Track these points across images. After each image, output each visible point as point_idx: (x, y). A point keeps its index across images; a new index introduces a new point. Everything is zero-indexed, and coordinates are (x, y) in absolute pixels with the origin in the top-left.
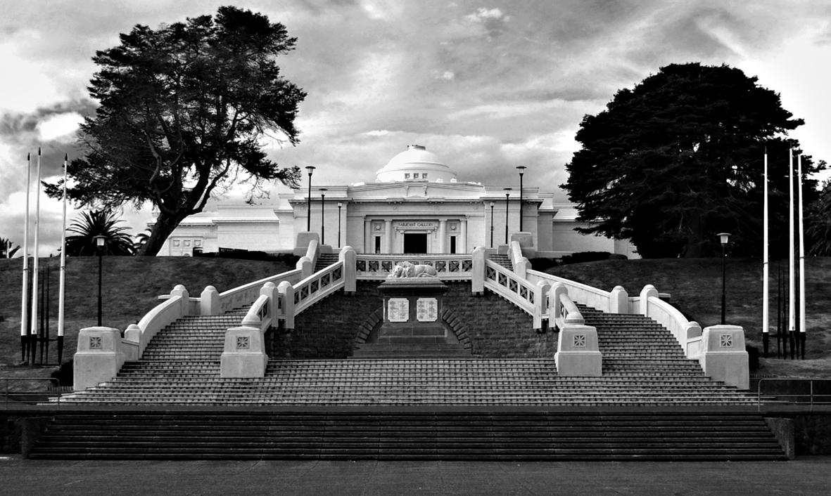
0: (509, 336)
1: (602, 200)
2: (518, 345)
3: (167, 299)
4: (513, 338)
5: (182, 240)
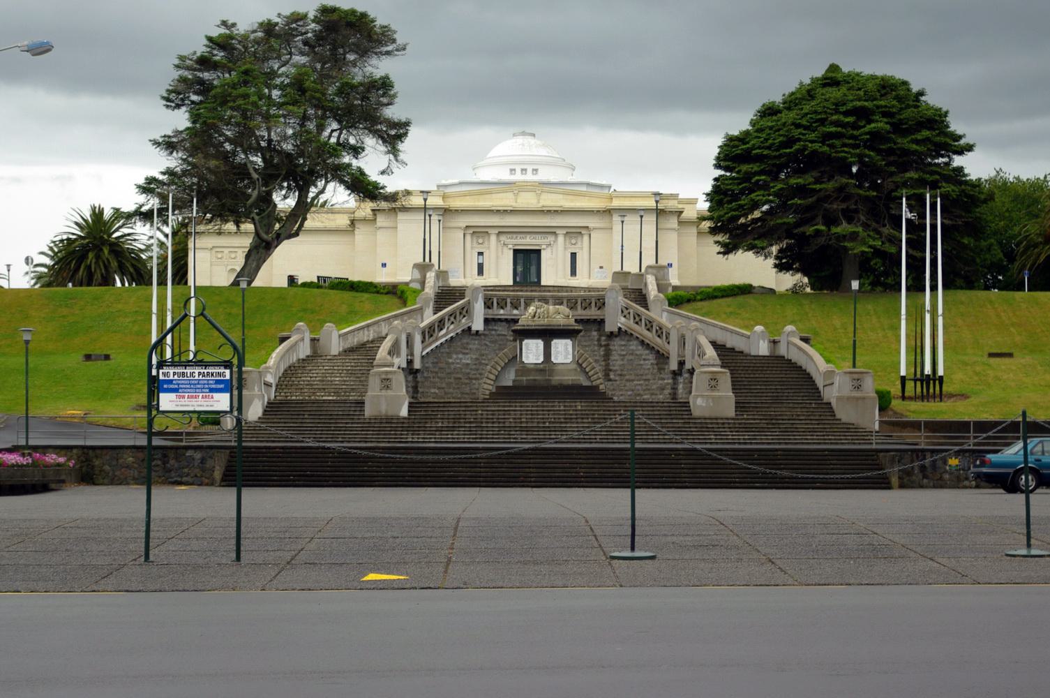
0: (644, 377)
1: (750, 229)
2: (654, 387)
4: (648, 380)
5: (226, 251)
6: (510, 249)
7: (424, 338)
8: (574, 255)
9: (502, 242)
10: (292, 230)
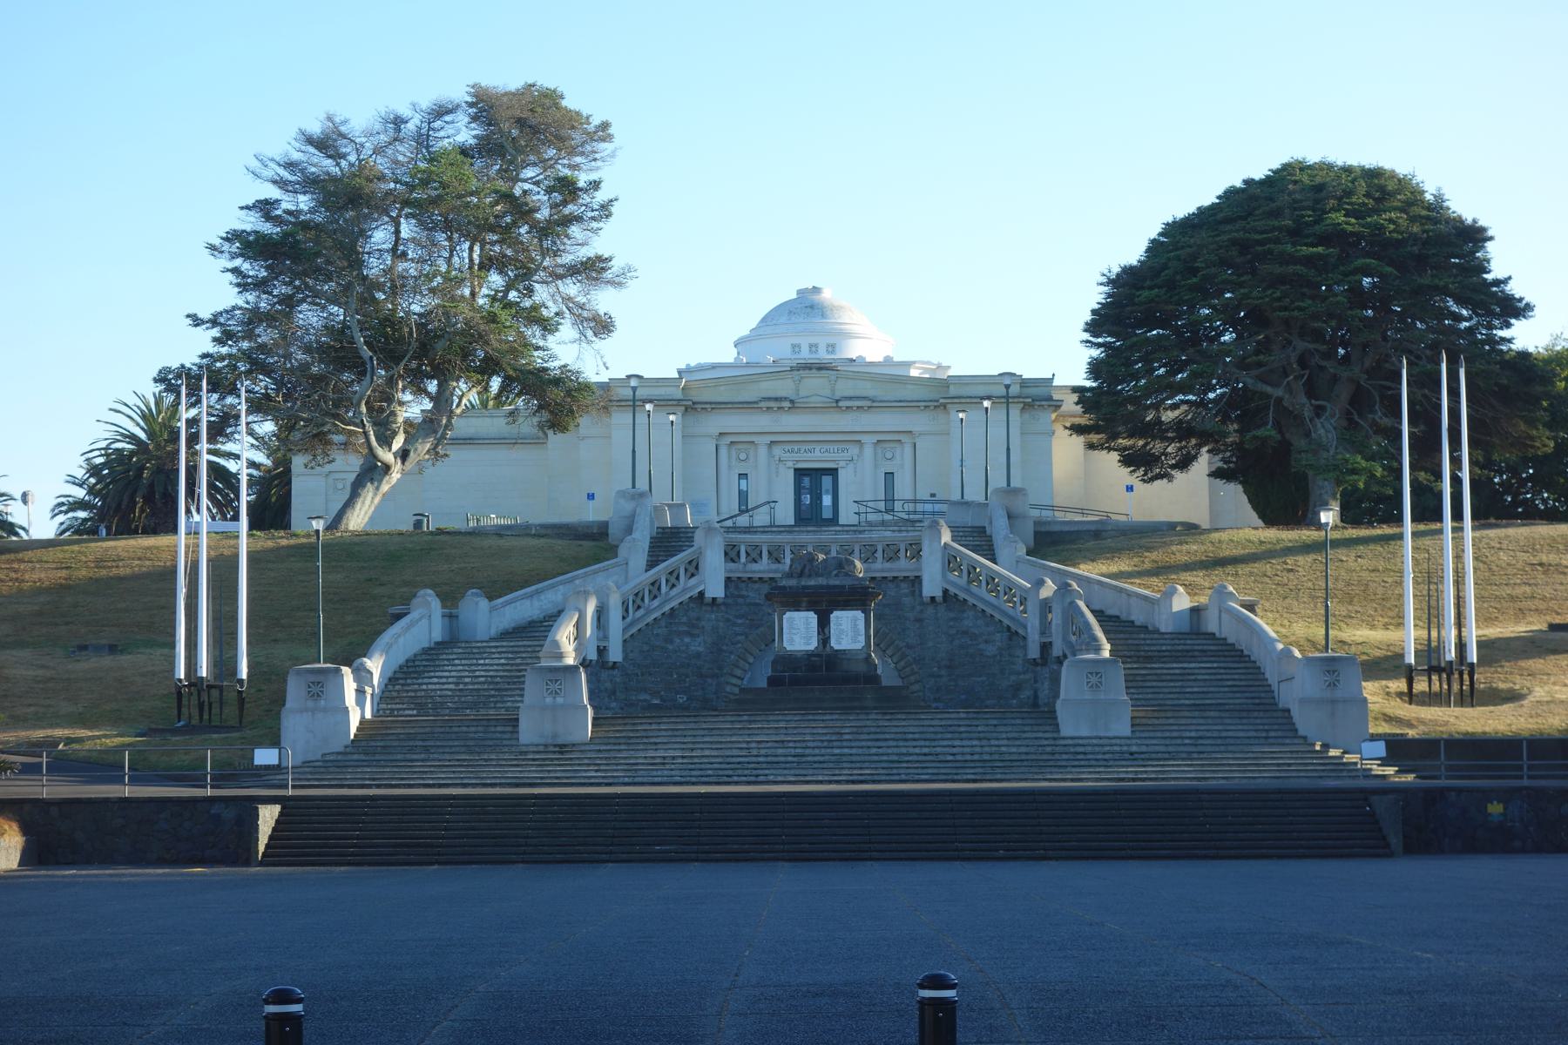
3: (406, 614)
7: (627, 610)
8: (889, 476)
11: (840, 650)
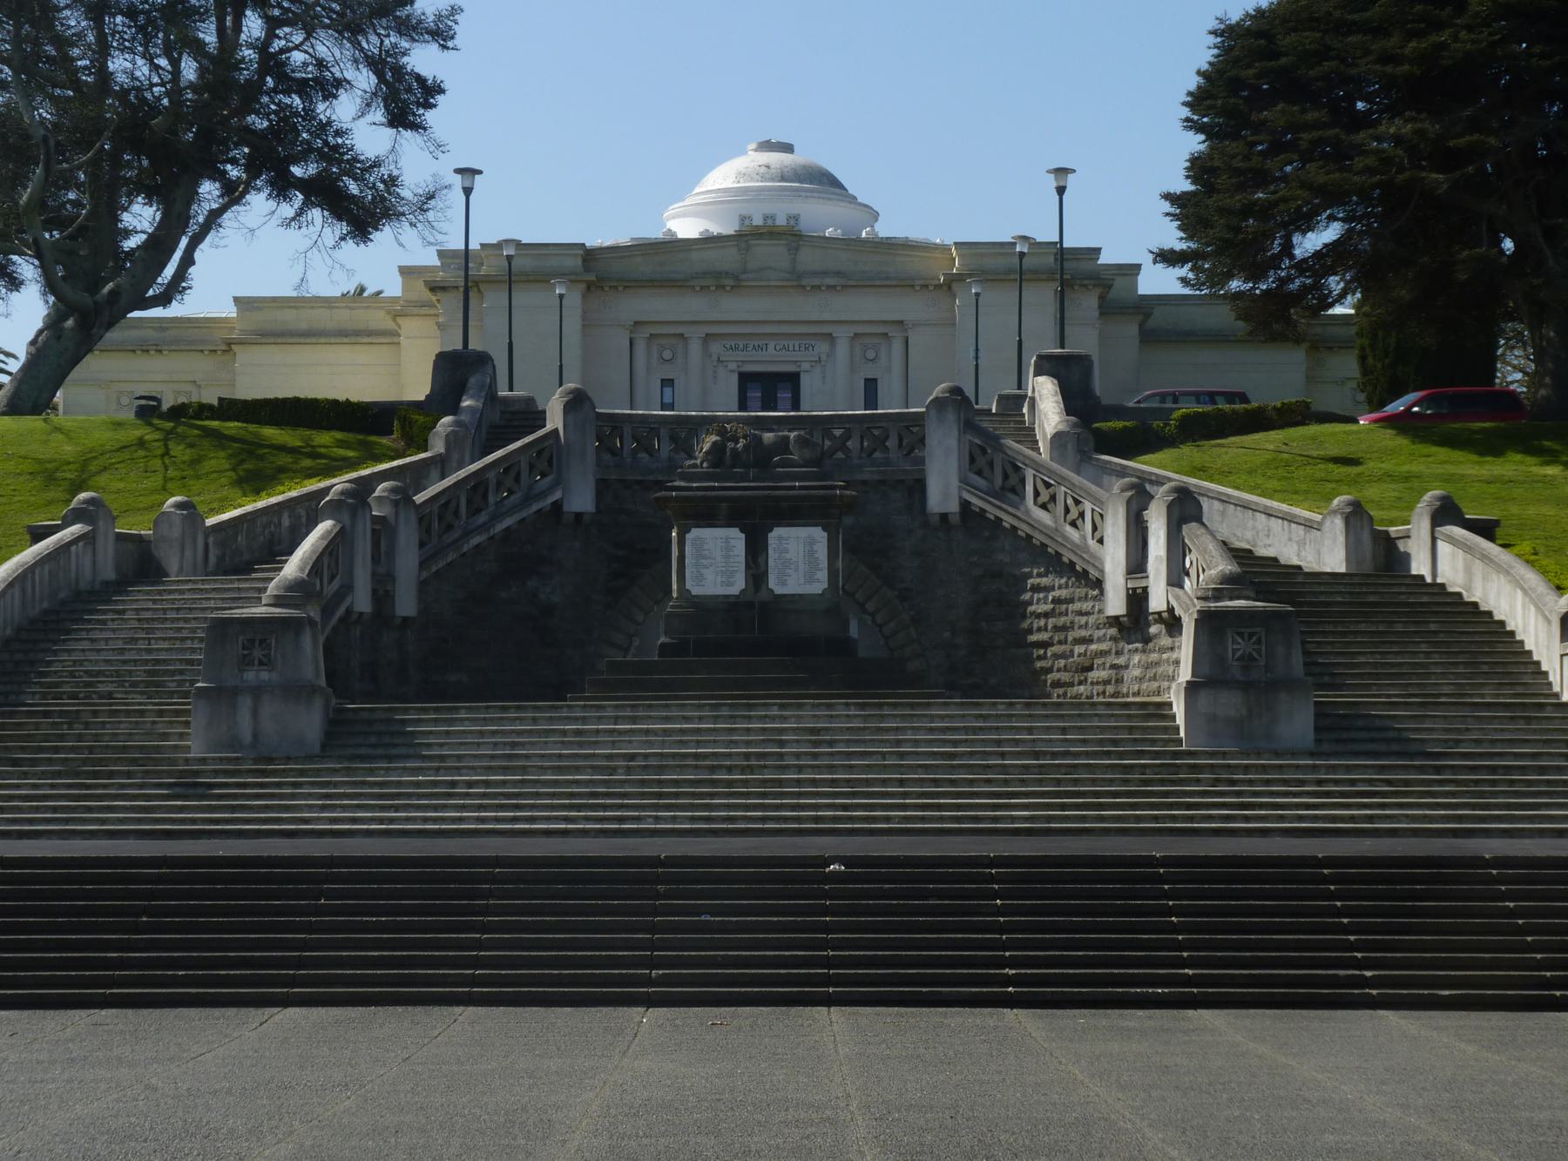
6: (731, 371)
7: (428, 531)
9: (715, 357)
10: (154, 281)
11: (785, 595)
